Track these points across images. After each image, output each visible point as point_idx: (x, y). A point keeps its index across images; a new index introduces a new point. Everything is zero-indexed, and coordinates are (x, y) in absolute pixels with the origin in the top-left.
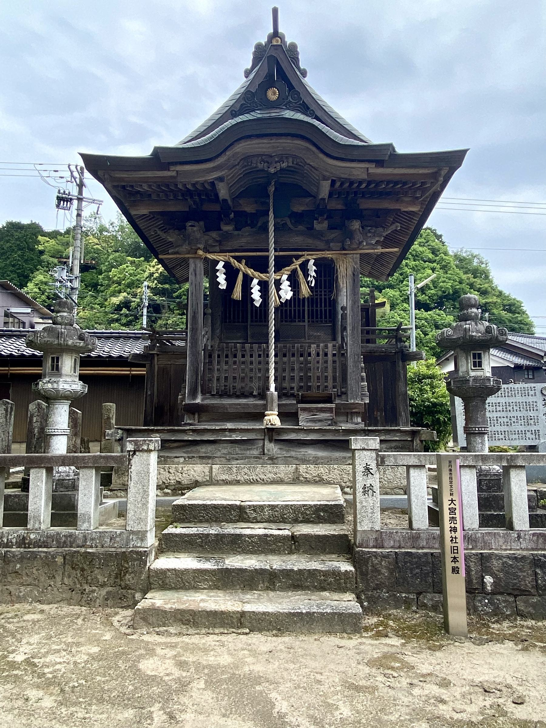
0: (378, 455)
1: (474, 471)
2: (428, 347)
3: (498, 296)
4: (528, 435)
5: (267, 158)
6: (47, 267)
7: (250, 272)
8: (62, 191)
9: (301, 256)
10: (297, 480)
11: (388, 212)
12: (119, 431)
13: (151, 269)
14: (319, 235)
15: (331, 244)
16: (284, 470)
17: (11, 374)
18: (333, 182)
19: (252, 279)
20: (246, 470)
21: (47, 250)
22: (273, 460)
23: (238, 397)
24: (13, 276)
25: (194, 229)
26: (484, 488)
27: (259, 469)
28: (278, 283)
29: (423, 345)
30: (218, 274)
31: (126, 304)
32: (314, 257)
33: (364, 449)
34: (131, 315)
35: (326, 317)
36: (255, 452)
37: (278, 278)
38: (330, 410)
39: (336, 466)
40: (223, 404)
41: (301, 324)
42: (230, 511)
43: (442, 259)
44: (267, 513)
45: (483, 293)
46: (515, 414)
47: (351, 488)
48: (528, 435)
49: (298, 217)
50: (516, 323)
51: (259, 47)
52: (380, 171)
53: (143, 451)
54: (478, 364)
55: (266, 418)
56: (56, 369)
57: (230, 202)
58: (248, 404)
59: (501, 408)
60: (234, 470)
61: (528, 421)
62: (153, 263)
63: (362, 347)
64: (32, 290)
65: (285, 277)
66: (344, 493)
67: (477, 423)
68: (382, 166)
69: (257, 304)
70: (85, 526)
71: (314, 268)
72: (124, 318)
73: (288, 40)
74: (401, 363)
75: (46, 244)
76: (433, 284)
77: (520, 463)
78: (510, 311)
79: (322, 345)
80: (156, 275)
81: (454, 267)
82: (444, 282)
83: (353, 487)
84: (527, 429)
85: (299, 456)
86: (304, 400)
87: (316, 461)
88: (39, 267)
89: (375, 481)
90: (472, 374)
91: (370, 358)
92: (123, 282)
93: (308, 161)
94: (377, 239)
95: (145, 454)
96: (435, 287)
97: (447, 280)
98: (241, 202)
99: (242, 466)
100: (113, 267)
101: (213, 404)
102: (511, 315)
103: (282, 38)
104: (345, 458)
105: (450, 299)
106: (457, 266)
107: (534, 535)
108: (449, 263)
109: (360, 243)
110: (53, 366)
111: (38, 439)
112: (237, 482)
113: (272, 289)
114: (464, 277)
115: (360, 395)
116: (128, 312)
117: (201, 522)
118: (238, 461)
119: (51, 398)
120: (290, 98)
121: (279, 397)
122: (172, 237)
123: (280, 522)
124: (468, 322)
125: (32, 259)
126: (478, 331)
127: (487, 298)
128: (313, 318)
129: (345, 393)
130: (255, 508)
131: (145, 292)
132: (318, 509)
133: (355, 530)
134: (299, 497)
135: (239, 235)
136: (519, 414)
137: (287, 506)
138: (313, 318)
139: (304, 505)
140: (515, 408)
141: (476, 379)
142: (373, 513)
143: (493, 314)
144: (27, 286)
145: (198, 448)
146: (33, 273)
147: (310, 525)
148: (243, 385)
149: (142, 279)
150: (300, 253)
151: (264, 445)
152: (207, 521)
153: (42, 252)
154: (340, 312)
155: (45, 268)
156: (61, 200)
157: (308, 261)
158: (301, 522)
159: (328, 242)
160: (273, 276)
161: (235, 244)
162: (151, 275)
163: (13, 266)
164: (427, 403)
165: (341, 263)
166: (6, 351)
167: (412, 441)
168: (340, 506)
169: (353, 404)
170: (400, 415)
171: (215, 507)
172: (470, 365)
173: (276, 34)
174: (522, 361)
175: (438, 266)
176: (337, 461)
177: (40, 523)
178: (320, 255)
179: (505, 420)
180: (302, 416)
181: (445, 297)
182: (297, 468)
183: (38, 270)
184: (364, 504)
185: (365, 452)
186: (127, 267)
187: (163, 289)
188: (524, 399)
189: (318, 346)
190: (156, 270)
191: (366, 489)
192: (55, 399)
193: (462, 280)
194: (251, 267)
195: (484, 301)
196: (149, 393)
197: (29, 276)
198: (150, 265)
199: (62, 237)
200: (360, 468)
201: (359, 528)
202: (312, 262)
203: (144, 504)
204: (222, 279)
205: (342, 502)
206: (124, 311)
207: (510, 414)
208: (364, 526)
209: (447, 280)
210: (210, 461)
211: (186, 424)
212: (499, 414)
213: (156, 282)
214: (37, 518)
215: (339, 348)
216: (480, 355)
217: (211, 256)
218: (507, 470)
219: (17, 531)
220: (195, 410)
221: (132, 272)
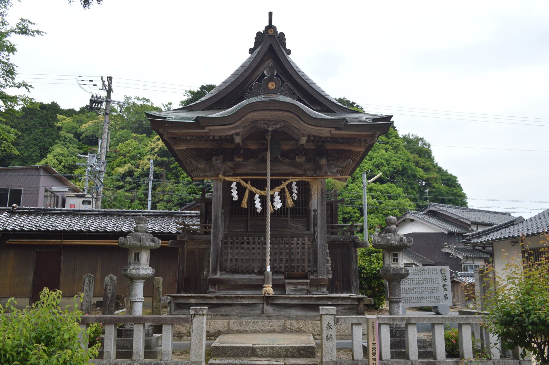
0: (335, 318)
1: (388, 327)
2: (382, 213)
3: (438, 172)
4: (433, 299)
5: (268, 122)
6: (64, 141)
7: (254, 189)
8: (95, 96)
9: (287, 179)
10: (285, 330)
11: (344, 151)
12: (169, 298)
13: (152, 144)
14: (298, 166)
15: (307, 172)
16: (276, 324)
17: (64, 245)
18: (309, 136)
19: (254, 194)
20: (252, 324)
21: (64, 127)
22: (269, 317)
23: (244, 273)
24: (35, 148)
25: (217, 162)
26: (398, 335)
27: (260, 323)
28: (272, 197)
29: (378, 212)
30: (232, 190)
31: (130, 173)
32: (296, 180)
33: (327, 314)
34: (134, 183)
35: (303, 214)
36: (258, 312)
37: (272, 193)
38: (306, 284)
39: (310, 321)
40: (234, 279)
41: (286, 218)
42: (246, 350)
43: (394, 142)
44: (269, 352)
45: (427, 170)
46: (424, 286)
47: (320, 335)
48: (433, 299)
49: (285, 154)
50: (452, 195)
51: (259, 34)
52: (338, 132)
53: (200, 315)
54: (396, 260)
55: (264, 289)
56: (137, 259)
57: (241, 144)
58: (251, 279)
59: (415, 282)
60: (244, 324)
61: (432, 290)
62: (154, 139)
63: (327, 237)
64: (51, 160)
65: (277, 193)
66: (315, 339)
67: (395, 295)
68: (340, 130)
69: (259, 211)
70: (166, 358)
71: (296, 187)
72: (128, 185)
73: (279, 30)
74: (353, 249)
75: (64, 122)
76: (387, 162)
77: (413, 322)
78: (447, 184)
79: (301, 239)
80: (156, 150)
81: (404, 148)
82: (395, 160)
83: (321, 335)
84: (431, 296)
85: (286, 315)
86: (289, 278)
87: (297, 318)
88: (57, 141)
89: (333, 332)
90: (392, 266)
91: (332, 245)
92: (128, 155)
93: (293, 125)
94: (337, 169)
95: (201, 317)
96: (388, 165)
97: (397, 159)
98: (248, 143)
99: (249, 321)
100: (119, 142)
101: (228, 278)
102: (448, 188)
103: (274, 28)
104: (316, 316)
105: (400, 174)
106: (405, 147)
107: (420, 362)
108: (399, 145)
109: (326, 173)
110: (135, 258)
111: (111, 301)
112: (246, 332)
113: (269, 202)
114: (411, 156)
115: (326, 273)
116: (131, 180)
117: (229, 357)
118: (246, 318)
119: (132, 279)
120: (282, 88)
121: (273, 274)
122: (202, 165)
123: (277, 357)
124: (390, 234)
125: (52, 135)
126: (395, 240)
127: (429, 174)
128: (293, 214)
129: (316, 271)
130: (261, 349)
131: (148, 163)
132: (299, 349)
133: (322, 362)
134: (287, 342)
135: (246, 164)
136: (427, 286)
137: (281, 347)
138: (293, 214)
139: (292, 347)
140: (424, 282)
141: (394, 269)
142: (332, 351)
143: (434, 188)
144: (46, 157)
145: (220, 309)
146: (52, 146)
147: (295, 359)
148: (248, 264)
149: (144, 152)
150: (287, 178)
151: (263, 307)
152: (232, 356)
153: (60, 129)
154: (313, 213)
155: (62, 142)
156: (94, 102)
157: (292, 182)
158: (290, 357)
159: (305, 170)
160: (268, 192)
161: (244, 170)
162: (153, 149)
163: (36, 140)
164: (374, 272)
165: (314, 184)
166: (59, 227)
167: (358, 305)
168: (313, 347)
169: (321, 279)
170: (353, 285)
171: (238, 348)
172: (391, 260)
173: (270, 27)
174: (454, 228)
175: (391, 147)
176: (311, 318)
177: (140, 356)
178: (300, 179)
179: (418, 290)
180: (288, 288)
181: (396, 173)
182: (284, 323)
183: (56, 144)
184: (327, 346)
185: (328, 316)
186: (132, 142)
187: (162, 161)
188: (430, 276)
189: (298, 240)
190: (157, 146)
191: (328, 338)
192: (136, 279)
193: (410, 159)
194: (253, 186)
195: (427, 177)
196: (181, 268)
197: (48, 148)
198: (151, 141)
199: (77, 116)
200: (325, 325)
201: (324, 360)
202: (294, 183)
203: (200, 346)
204: (235, 194)
205: (314, 345)
206: (128, 179)
207: (421, 286)
208: (326, 359)
209: (397, 159)
210: (228, 318)
211: (210, 292)
212: (414, 286)
213: (156, 155)
214: (138, 353)
215: (312, 241)
216: (397, 254)
217: (228, 179)
218: (407, 325)
219: (127, 361)
220: (217, 283)
221: (135, 146)
